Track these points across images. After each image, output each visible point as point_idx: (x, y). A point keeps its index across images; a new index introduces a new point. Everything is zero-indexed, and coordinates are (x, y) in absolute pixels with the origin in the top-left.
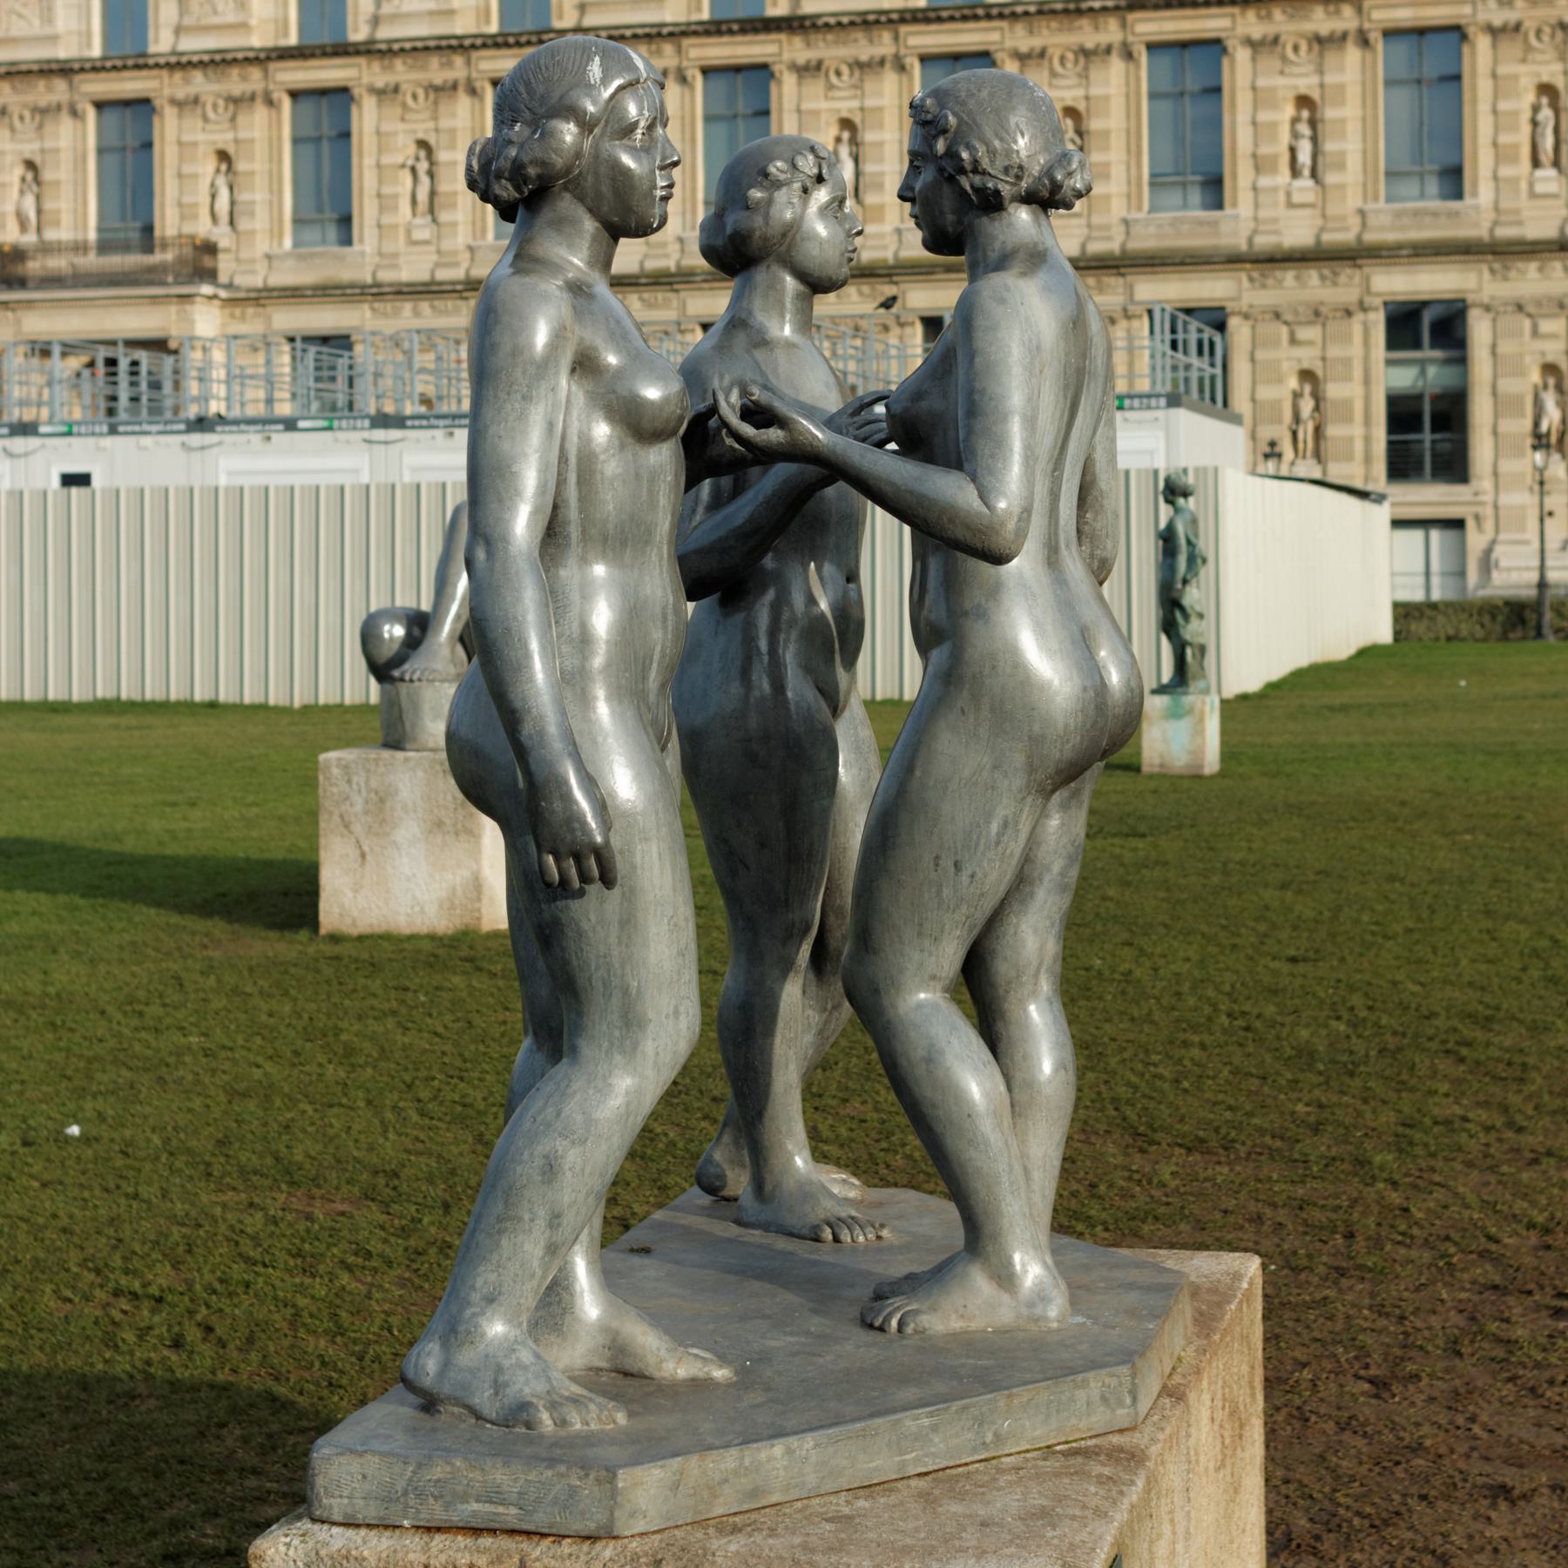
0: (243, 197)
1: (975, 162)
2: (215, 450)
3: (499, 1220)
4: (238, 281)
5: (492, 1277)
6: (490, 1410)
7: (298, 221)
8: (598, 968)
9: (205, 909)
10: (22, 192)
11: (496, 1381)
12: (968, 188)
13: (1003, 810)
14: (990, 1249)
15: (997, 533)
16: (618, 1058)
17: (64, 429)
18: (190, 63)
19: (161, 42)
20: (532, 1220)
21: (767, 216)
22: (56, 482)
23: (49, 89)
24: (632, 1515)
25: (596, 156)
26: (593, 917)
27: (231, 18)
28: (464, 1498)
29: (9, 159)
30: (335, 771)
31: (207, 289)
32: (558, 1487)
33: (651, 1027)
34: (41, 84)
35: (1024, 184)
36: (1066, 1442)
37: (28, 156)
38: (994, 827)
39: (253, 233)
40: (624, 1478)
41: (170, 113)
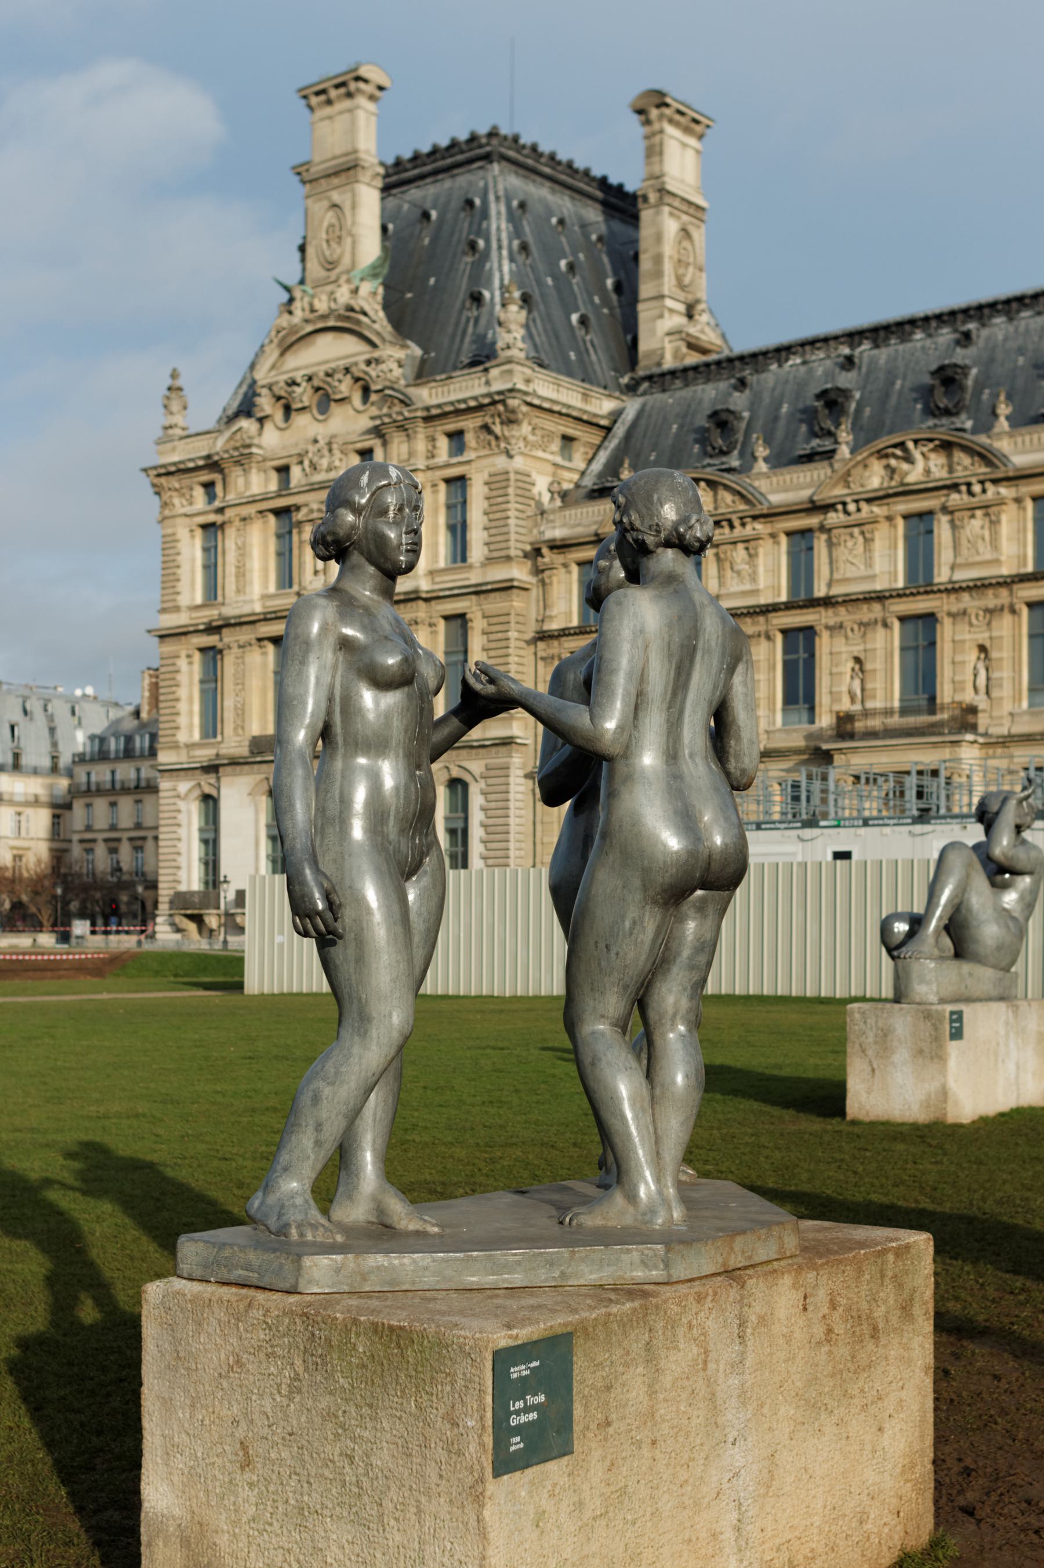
0: (995, 675)
1: (631, 523)
2: (930, 836)
4: (991, 731)
5: (287, 1157)
6: (273, 1229)
7: (1032, 690)
10: (852, 678)
13: (632, 913)
16: (356, 1038)
17: (835, 823)
18: (961, 588)
19: (942, 575)
21: (608, 576)
22: (830, 857)
23: (870, 610)
24: (310, 1282)
25: (366, 528)
27: (988, 556)
28: (236, 1267)
29: (844, 656)
30: (857, 1016)
31: (970, 737)
34: (865, 607)
35: (662, 536)
37: (856, 654)
38: (627, 924)
39: (1001, 698)
40: (307, 1261)
41: (947, 622)
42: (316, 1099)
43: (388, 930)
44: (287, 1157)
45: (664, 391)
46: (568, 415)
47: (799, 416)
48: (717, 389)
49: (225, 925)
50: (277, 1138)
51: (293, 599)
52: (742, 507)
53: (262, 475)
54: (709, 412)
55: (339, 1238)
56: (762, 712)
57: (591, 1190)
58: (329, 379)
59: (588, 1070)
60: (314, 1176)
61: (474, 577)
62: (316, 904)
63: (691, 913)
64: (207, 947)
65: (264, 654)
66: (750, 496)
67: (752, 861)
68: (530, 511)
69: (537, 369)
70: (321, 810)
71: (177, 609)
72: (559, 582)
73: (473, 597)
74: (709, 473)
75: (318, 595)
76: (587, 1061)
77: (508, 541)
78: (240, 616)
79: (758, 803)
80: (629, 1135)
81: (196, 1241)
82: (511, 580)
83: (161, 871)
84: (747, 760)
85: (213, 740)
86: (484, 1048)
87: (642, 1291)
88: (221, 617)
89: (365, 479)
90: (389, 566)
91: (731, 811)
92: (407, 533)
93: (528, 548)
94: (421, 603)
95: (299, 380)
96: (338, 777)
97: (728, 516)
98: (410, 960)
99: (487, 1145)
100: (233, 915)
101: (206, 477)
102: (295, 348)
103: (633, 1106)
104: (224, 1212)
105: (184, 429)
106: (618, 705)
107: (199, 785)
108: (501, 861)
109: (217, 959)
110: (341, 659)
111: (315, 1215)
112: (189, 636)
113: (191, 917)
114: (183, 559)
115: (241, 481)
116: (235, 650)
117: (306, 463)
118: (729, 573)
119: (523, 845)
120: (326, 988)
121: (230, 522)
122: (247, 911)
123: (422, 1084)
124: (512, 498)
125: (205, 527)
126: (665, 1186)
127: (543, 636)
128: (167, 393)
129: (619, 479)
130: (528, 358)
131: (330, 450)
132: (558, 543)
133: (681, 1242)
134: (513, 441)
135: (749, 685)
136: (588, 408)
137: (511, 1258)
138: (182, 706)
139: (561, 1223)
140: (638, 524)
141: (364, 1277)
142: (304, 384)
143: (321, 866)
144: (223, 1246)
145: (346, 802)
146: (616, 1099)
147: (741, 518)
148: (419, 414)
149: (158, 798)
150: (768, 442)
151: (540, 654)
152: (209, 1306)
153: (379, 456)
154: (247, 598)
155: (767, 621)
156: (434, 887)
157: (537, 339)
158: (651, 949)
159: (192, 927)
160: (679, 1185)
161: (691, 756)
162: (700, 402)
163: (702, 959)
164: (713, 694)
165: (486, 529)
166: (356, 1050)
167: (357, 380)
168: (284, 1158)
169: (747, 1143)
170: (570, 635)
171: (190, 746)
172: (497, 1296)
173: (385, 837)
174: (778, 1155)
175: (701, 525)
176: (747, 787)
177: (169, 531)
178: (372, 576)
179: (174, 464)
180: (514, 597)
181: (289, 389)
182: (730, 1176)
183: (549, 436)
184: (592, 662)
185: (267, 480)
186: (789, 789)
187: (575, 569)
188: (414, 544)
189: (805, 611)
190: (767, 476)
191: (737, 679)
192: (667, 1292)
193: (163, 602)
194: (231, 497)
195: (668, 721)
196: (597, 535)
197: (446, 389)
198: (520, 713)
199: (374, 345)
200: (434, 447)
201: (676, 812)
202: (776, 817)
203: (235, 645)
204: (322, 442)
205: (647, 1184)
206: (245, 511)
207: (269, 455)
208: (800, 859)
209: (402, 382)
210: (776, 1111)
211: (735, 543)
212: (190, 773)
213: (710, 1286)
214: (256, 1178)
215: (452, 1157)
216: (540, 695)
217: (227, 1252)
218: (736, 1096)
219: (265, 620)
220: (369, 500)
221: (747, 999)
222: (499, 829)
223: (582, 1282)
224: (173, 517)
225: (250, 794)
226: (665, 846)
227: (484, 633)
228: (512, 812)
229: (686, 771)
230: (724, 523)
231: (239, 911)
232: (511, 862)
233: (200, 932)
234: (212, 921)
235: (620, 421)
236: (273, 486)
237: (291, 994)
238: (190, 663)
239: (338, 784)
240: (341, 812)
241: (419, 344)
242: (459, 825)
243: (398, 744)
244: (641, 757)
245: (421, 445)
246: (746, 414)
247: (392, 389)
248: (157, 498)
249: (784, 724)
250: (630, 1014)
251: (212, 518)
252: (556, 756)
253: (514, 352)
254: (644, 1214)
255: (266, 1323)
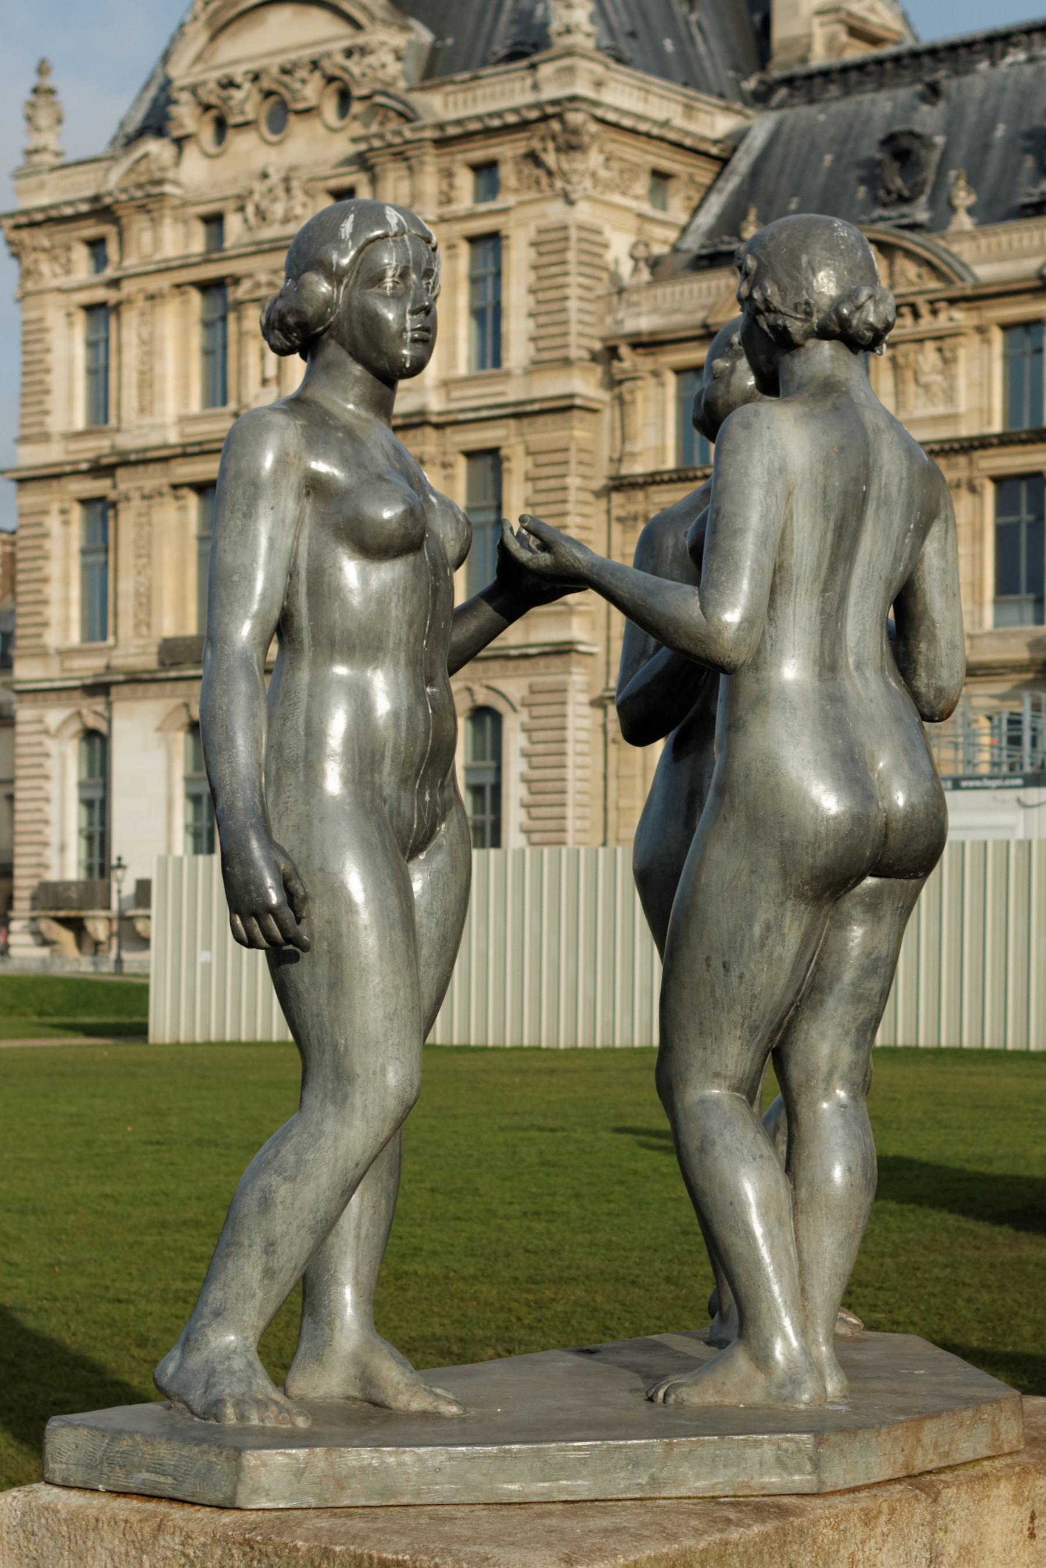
1: (766, 301)
3: (228, 1245)
5: (220, 1294)
6: (197, 1407)
8: (313, 1027)
9: (998, 1219)
11: (207, 1382)
12: (765, 327)
13: (765, 913)
14: (751, 1331)
15: (715, 641)
16: (330, 1108)
20: (250, 1246)
21: (728, 385)
24: (255, 1491)
26: (306, 980)
32: (201, 1462)
33: (359, 1081)
35: (815, 320)
36: (735, 1496)
38: (757, 930)
40: (251, 1458)
42: (266, 1203)
43: (381, 938)
44: (220, 1294)
45: (811, 101)
46: (661, 139)
47: (1022, 143)
48: (894, 100)
49: (119, 935)
50: (201, 1268)
51: (228, 424)
52: (933, 284)
53: (180, 228)
54: (881, 135)
55: (302, 1423)
56: (966, 606)
57: (697, 1349)
58: (286, 79)
59: (695, 1159)
60: (262, 1324)
61: (513, 391)
62: (267, 896)
63: (857, 913)
64: (90, 969)
65: (183, 509)
66: (945, 269)
67: (951, 836)
68: (602, 288)
69: (613, 65)
70: (276, 747)
71: (45, 437)
72: (646, 400)
73: (512, 423)
74: (883, 231)
75: (272, 409)
76: (692, 1144)
77: (565, 334)
78: (146, 450)
79: (956, 746)
80: (758, 1261)
81: (76, 1427)
82: (571, 396)
83: (18, 850)
84: (945, 673)
85: (100, 644)
86: (525, 1129)
87: (778, 1506)
88: (114, 451)
89: (347, 227)
90: (384, 364)
91: (921, 753)
92: (413, 312)
93: (598, 346)
94: (429, 431)
95: (238, 79)
96: (303, 695)
97: (911, 299)
98: (415, 985)
99: (531, 1280)
100: (131, 919)
101: (92, 230)
102: (233, 28)
103: (764, 1216)
104: (116, 1383)
105: (58, 154)
106: (745, 585)
107: (79, 714)
108: (554, 836)
109: (107, 988)
110: (308, 509)
111: (263, 1385)
112: (64, 481)
113: (66, 923)
114: (56, 359)
115: (147, 237)
116: (137, 503)
117: (250, 210)
118: (911, 388)
119: (588, 811)
120: (278, 1030)
121: (129, 301)
122: (153, 911)
123: (428, 1185)
124: (572, 267)
125: (91, 309)
126: (815, 1341)
127: (621, 484)
128: (31, 97)
129: (741, 240)
130: (599, 48)
131: (288, 190)
132: (645, 339)
133: (839, 1429)
134: (575, 178)
135: (950, 555)
136: (693, 127)
137: (572, 1455)
138: (53, 591)
139: (651, 1399)
140: (776, 301)
141: (341, 1484)
142: (247, 86)
143: (275, 836)
144: (118, 1434)
145: (315, 735)
146: (737, 1204)
147: (931, 302)
148: (428, 134)
149: (14, 735)
150: (973, 183)
151: (616, 512)
152: (96, 1528)
153: (364, 193)
154: (156, 420)
155: (971, 463)
156: (454, 869)
157: (613, 18)
158: (794, 970)
159: (66, 937)
160: (837, 1342)
161: (858, 666)
162: (868, 119)
163: (874, 985)
164: (894, 570)
165: (532, 315)
166: (329, 1126)
167: (330, 79)
168: (215, 1296)
169: (938, 1279)
170: (662, 482)
171: (64, 653)
172: (550, 1514)
173: (376, 790)
174: (986, 1297)
175: (876, 304)
176: (944, 716)
177: (34, 315)
178: (357, 380)
179: (43, 209)
180: (576, 423)
181: (224, 93)
182: (911, 1328)
183: (631, 170)
184: (703, 520)
185: (188, 237)
186: (1004, 726)
187: (671, 380)
188: (425, 329)
189: (1030, 448)
190: (972, 237)
191: (931, 546)
192: (817, 1507)
193: (24, 426)
194: (132, 262)
195: (823, 611)
196: (705, 326)
197: (470, 95)
198: (589, 600)
199: (357, 26)
200: (451, 186)
201: (834, 754)
202: (984, 769)
203: (136, 496)
204: (275, 178)
205: (785, 1338)
206: (154, 284)
207: (190, 196)
208: (1020, 835)
209: (402, 84)
210: (983, 1229)
211: (920, 341)
212: (64, 695)
213: (884, 1499)
214: (167, 1330)
215: (476, 1298)
216: (621, 569)
217: (124, 1445)
218: (920, 1204)
219: (184, 455)
220: (354, 260)
221: (937, 1053)
222: (550, 786)
223: (683, 1492)
224: (40, 292)
225: (159, 729)
226: (817, 807)
227: (528, 478)
228: (570, 760)
229: (849, 689)
230: (905, 310)
231: (141, 912)
232: (570, 837)
233: (79, 944)
234: (99, 928)
235: (742, 148)
236: (198, 245)
237: (222, 1044)
238: (66, 523)
239: (302, 708)
240: (307, 751)
241: (429, 24)
242: (488, 779)
243: (398, 645)
244: (779, 666)
245: (430, 183)
246: (940, 140)
247: (385, 94)
248: (13, 263)
249: (997, 624)
250: (760, 1071)
251: (101, 295)
252: (645, 666)
253: (577, 40)
254: (781, 1386)
255: (186, 1556)
